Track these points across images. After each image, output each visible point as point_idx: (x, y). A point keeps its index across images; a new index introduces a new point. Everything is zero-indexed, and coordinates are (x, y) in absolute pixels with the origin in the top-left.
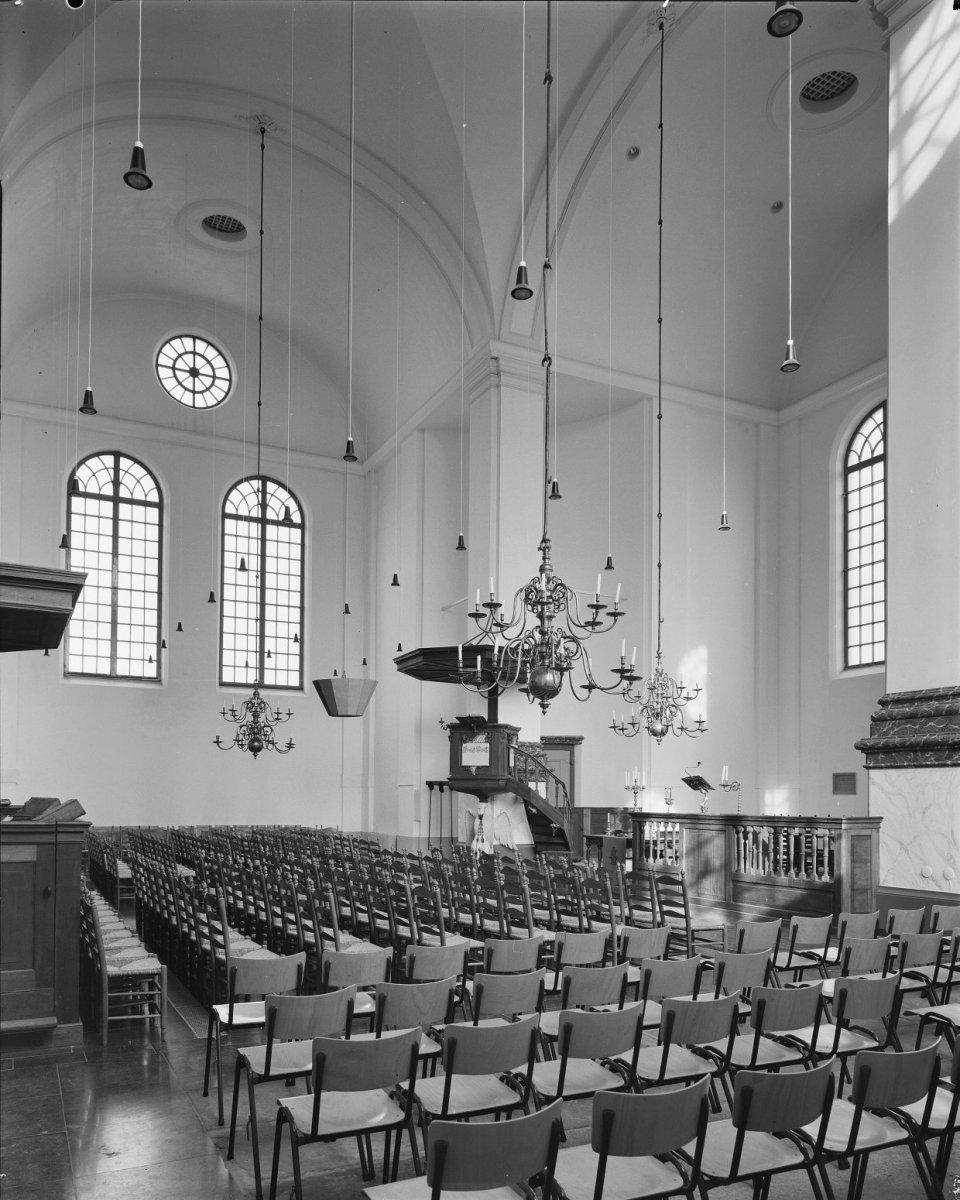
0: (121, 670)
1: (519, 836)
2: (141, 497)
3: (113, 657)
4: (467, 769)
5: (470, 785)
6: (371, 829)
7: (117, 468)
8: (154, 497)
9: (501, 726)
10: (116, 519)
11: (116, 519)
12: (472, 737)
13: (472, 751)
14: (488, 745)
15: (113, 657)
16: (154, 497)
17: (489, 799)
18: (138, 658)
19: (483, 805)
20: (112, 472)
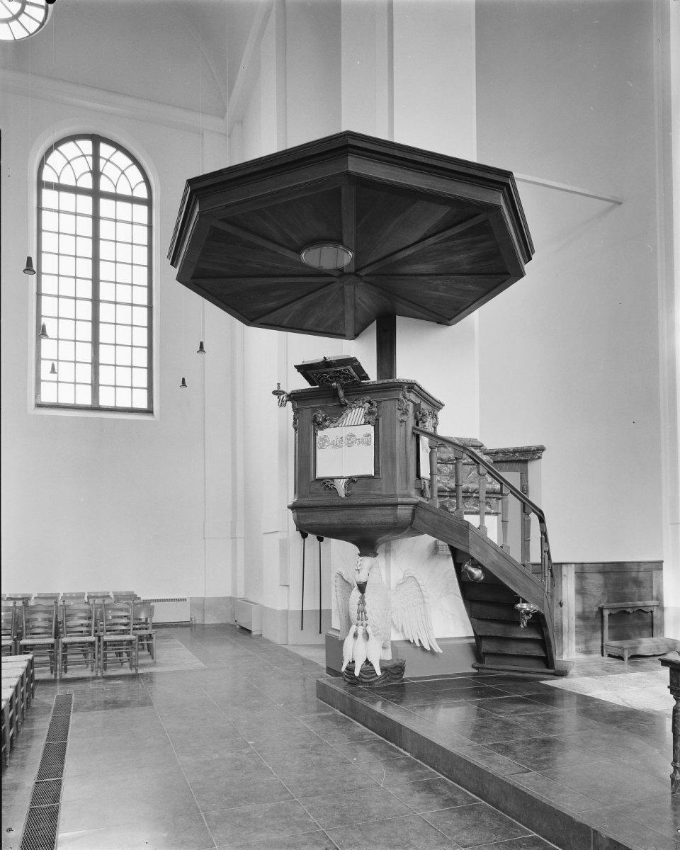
0: (106, 400)
1: (445, 622)
2: (127, 192)
3: (95, 385)
4: (327, 483)
5: (335, 518)
6: (241, 594)
7: (96, 156)
8: (142, 192)
9: (400, 386)
10: (96, 218)
11: (96, 218)
12: (338, 410)
13: (337, 445)
14: (370, 429)
15: (95, 385)
16: (142, 192)
17: (380, 550)
18: (125, 386)
19: (367, 561)
20: (90, 159)
